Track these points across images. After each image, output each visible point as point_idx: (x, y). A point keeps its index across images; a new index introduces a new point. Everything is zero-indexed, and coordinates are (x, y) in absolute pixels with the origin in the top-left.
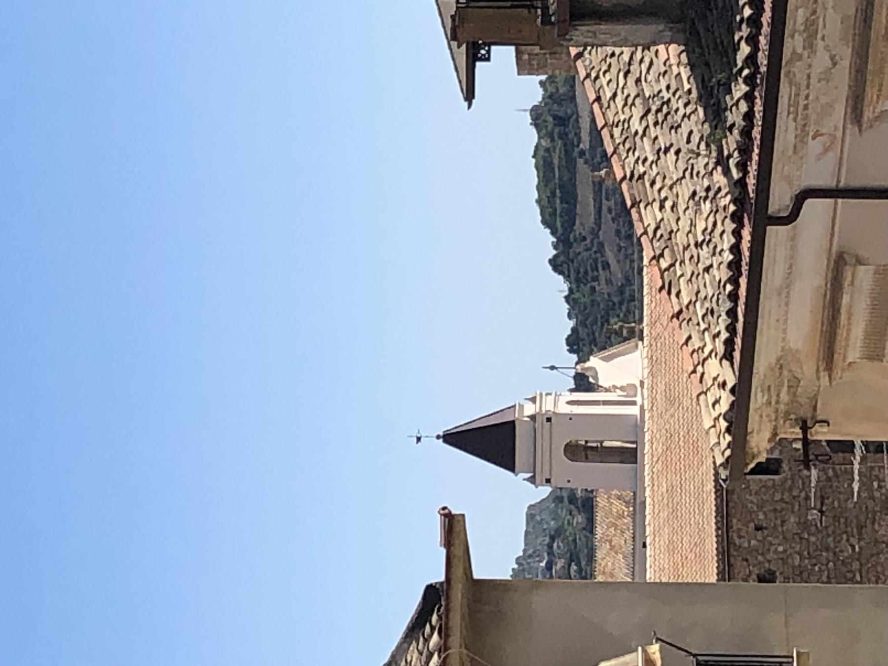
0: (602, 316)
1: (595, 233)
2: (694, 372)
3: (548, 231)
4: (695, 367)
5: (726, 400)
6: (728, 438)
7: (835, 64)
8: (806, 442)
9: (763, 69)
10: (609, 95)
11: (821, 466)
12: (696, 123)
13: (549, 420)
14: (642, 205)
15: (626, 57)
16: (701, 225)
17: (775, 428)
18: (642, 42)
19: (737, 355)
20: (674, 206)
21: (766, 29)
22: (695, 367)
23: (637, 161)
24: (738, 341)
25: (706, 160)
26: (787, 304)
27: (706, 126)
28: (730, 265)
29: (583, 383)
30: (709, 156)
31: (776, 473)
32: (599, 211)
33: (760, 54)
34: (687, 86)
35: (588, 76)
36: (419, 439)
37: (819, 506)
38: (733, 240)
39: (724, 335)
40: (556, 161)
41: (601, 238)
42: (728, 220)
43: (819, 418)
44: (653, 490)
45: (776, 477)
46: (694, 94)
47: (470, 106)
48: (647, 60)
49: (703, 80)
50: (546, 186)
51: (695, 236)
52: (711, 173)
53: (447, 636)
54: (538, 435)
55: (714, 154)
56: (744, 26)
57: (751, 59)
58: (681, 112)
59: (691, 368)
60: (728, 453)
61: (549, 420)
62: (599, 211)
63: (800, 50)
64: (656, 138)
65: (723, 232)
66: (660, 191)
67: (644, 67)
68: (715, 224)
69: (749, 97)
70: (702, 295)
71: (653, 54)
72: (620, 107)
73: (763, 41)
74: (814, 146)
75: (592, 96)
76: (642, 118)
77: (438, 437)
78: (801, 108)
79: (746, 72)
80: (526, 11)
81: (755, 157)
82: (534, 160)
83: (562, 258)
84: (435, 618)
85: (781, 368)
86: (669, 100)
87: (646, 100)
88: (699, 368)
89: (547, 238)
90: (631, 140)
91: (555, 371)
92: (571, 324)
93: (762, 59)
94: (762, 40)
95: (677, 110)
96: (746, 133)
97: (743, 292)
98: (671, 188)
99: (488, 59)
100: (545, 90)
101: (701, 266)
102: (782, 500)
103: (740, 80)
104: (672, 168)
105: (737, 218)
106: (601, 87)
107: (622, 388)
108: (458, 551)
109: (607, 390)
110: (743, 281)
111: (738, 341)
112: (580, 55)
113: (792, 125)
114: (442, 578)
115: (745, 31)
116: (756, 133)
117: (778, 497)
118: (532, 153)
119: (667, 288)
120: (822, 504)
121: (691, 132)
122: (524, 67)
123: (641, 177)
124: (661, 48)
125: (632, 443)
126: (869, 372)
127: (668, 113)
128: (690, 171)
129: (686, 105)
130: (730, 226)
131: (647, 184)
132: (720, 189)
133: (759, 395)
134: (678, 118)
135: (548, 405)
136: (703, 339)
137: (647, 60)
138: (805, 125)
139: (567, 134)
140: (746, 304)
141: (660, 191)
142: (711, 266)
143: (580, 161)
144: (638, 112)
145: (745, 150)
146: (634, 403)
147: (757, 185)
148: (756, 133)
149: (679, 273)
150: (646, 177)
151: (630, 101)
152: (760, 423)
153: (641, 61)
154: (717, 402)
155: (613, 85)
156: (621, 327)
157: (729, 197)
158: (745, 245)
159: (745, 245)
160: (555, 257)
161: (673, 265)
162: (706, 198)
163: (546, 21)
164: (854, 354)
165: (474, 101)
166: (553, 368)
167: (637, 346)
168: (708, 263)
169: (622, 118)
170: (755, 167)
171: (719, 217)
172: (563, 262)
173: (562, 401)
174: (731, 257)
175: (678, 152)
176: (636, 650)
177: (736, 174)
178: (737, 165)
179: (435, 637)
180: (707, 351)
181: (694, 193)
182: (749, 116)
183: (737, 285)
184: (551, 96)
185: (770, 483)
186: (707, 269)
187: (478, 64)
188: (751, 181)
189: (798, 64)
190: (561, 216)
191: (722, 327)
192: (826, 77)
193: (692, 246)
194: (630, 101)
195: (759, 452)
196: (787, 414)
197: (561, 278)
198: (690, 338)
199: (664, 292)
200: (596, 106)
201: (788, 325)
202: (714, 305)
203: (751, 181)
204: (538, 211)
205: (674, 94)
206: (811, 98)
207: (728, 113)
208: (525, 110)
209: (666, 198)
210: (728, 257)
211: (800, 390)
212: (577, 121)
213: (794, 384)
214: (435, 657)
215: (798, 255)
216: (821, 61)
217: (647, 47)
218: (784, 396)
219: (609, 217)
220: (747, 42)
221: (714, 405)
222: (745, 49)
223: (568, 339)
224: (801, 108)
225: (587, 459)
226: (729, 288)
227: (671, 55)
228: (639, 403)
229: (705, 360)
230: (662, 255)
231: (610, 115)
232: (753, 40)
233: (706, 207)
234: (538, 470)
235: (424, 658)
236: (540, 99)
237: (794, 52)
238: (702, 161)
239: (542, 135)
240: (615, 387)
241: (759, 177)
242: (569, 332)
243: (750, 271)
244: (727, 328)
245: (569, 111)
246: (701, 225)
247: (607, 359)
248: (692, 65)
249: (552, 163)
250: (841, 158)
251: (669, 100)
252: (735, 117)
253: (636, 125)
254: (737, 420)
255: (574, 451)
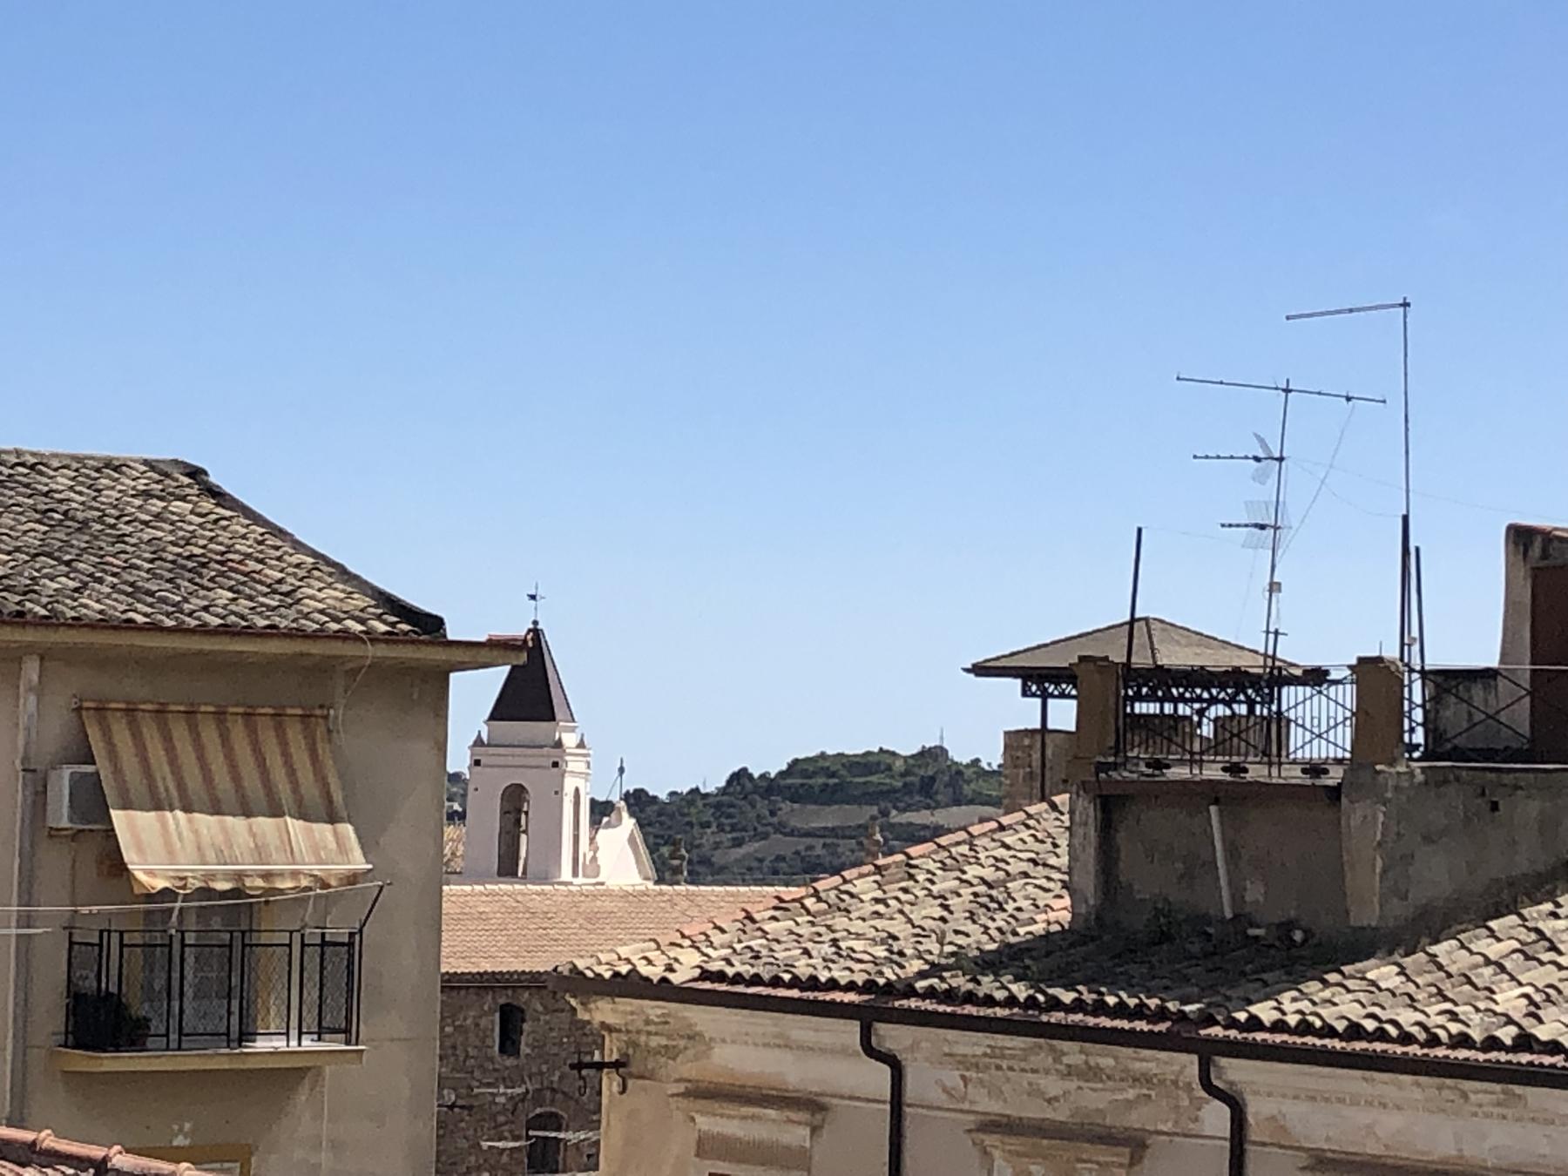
0: (686, 835)
1: (780, 828)
2: (683, 936)
3: (784, 767)
4: (688, 937)
5: (654, 972)
6: (607, 975)
7: (1049, 1101)
8: (600, 1066)
9: (1044, 1018)
10: (1008, 840)
11: (509, 1106)
12: (977, 939)
13: (555, 765)
14: (878, 878)
15: (1053, 861)
16: (858, 945)
17: (619, 1031)
18: (1075, 878)
19: (707, 985)
20: (877, 914)
21: (1091, 1021)
22: (688, 937)
23: (929, 872)
24: (723, 987)
25: (936, 952)
26: (766, 1045)
27: (976, 953)
28: (814, 978)
29: (601, 810)
30: (940, 955)
31: (502, 1050)
32: (808, 834)
33: (1062, 1014)
34: (1021, 931)
35: (1030, 816)
36: (533, 597)
37: (460, 1102)
38: (843, 982)
39: (730, 971)
40: (874, 779)
41: (773, 836)
42: (866, 977)
43: (630, 1083)
44: (482, 894)
45: (497, 1048)
46: (1012, 939)
47: (967, 670)
48: (1051, 885)
49: (1029, 950)
50: (843, 765)
51: (844, 939)
52: (920, 958)
53: (387, 642)
54: (529, 751)
55: (943, 961)
56: (1094, 996)
57: (1055, 1004)
58: (990, 924)
59: (687, 933)
60: (589, 974)
61: (555, 765)
62: (808, 834)
63: (1065, 1060)
64: (959, 895)
65: (852, 971)
66: (897, 899)
67: (1043, 882)
68: (860, 961)
69: (1011, 1001)
70: (775, 946)
71: (1057, 891)
72: (995, 853)
73: (1078, 1017)
74: (953, 1078)
75: (1005, 820)
76: (982, 879)
77: (535, 623)
78: (998, 1061)
79: (1041, 998)
80: (1112, 744)
81: (941, 1008)
82: (876, 750)
83: (749, 785)
84: (405, 627)
85: (690, 1038)
86: (1005, 910)
87: (1003, 883)
88: (687, 943)
89: (775, 766)
90: (954, 865)
91: (617, 773)
92: (663, 796)
93: (1057, 1017)
94: (1078, 1017)
95: (993, 920)
96: (970, 998)
97: (782, 992)
98: (901, 912)
99: (1024, 694)
100: (967, 766)
101: (809, 945)
102: (467, 1056)
103: (1031, 992)
104: (924, 913)
105: (870, 986)
106: (1017, 831)
107: (594, 859)
108: (485, 655)
109: (592, 840)
110: (795, 993)
111: (723, 987)
112: (1054, 807)
113: (979, 1051)
114: (450, 637)
115: (1089, 997)
116: (969, 1009)
117: (472, 1052)
118: (885, 747)
119: (781, 905)
120: (462, 1107)
121: (967, 935)
122: (1014, 740)
123: (911, 877)
124: (1067, 901)
125: (524, 872)
126: (681, 1142)
127: (988, 909)
128: (921, 934)
129: (999, 929)
130: (860, 979)
131: (903, 884)
132: (902, 967)
133: (659, 1012)
134: (984, 920)
135: (574, 764)
136: (722, 947)
137: (1051, 885)
138: (977, 1066)
139: (910, 793)
140: (768, 996)
141: (897, 899)
142: (810, 957)
143: (874, 810)
144: (989, 874)
145: (950, 996)
146: (575, 874)
147: (909, 1010)
148: (969, 1009)
149: (799, 920)
150: (911, 883)
151: (1001, 865)
152: (624, 1013)
153: (1049, 879)
154: (650, 962)
155: (1020, 846)
156: (682, 858)
157: (894, 978)
158: (838, 996)
159: (838, 996)
160: (750, 776)
161: (809, 913)
162: (892, 952)
163: (1102, 767)
164: (703, 1123)
165: (972, 676)
166: (622, 770)
167: (647, 879)
168: (814, 953)
169: (982, 856)
170: (930, 1008)
171: (869, 967)
172: (743, 787)
173: (582, 780)
174: (823, 980)
175: (943, 919)
176: (368, 862)
177: (921, 985)
178: (931, 987)
179: (383, 628)
180: (709, 951)
181: (896, 938)
182: (989, 1001)
183: (790, 986)
184: (959, 773)
185: (489, 1042)
186: (806, 952)
187: (1019, 682)
188: (913, 1003)
189: (1050, 1059)
190: (802, 785)
191: (739, 968)
192: (1035, 1092)
193: (832, 936)
194: (1001, 865)
195: (590, 1011)
196: (636, 1045)
197: (722, 784)
198: (723, 931)
199: (775, 903)
200: (994, 825)
201: (739, 1046)
202: (764, 960)
203: (913, 1003)
204: (811, 755)
205: (1012, 916)
206: (1010, 1074)
207: (992, 978)
208: (942, 738)
209: (887, 906)
210: (823, 976)
211: (663, 1060)
212: (928, 807)
213: (671, 1053)
214: (360, 628)
215: (826, 1058)
216: (1053, 1086)
217: (1065, 885)
218: (654, 1042)
219: (801, 848)
220: (1075, 1000)
221: (645, 958)
222: (1067, 997)
223: (642, 790)
224: (998, 1061)
225: (504, 813)
226: (787, 977)
227: (1060, 911)
228: (576, 881)
229: (698, 948)
230: (820, 900)
231: (985, 841)
232: (1078, 1006)
233: (881, 952)
234: (491, 750)
235: (357, 613)
236: (956, 759)
237: (1064, 1054)
238: (935, 948)
239: (911, 761)
240: (596, 850)
241: (918, 1011)
242: (651, 793)
243: (808, 1001)
244: (738, 975)
245: (939, 797)
246: (858, 945)
247: (632, 840)
248: (1048, 935)
249: (872, 774)
250: (939, 1108)
251: (1005, 910)
252: (987, 985)
253: (972, 872)
254: (629, 985)
255: (514, 800)
